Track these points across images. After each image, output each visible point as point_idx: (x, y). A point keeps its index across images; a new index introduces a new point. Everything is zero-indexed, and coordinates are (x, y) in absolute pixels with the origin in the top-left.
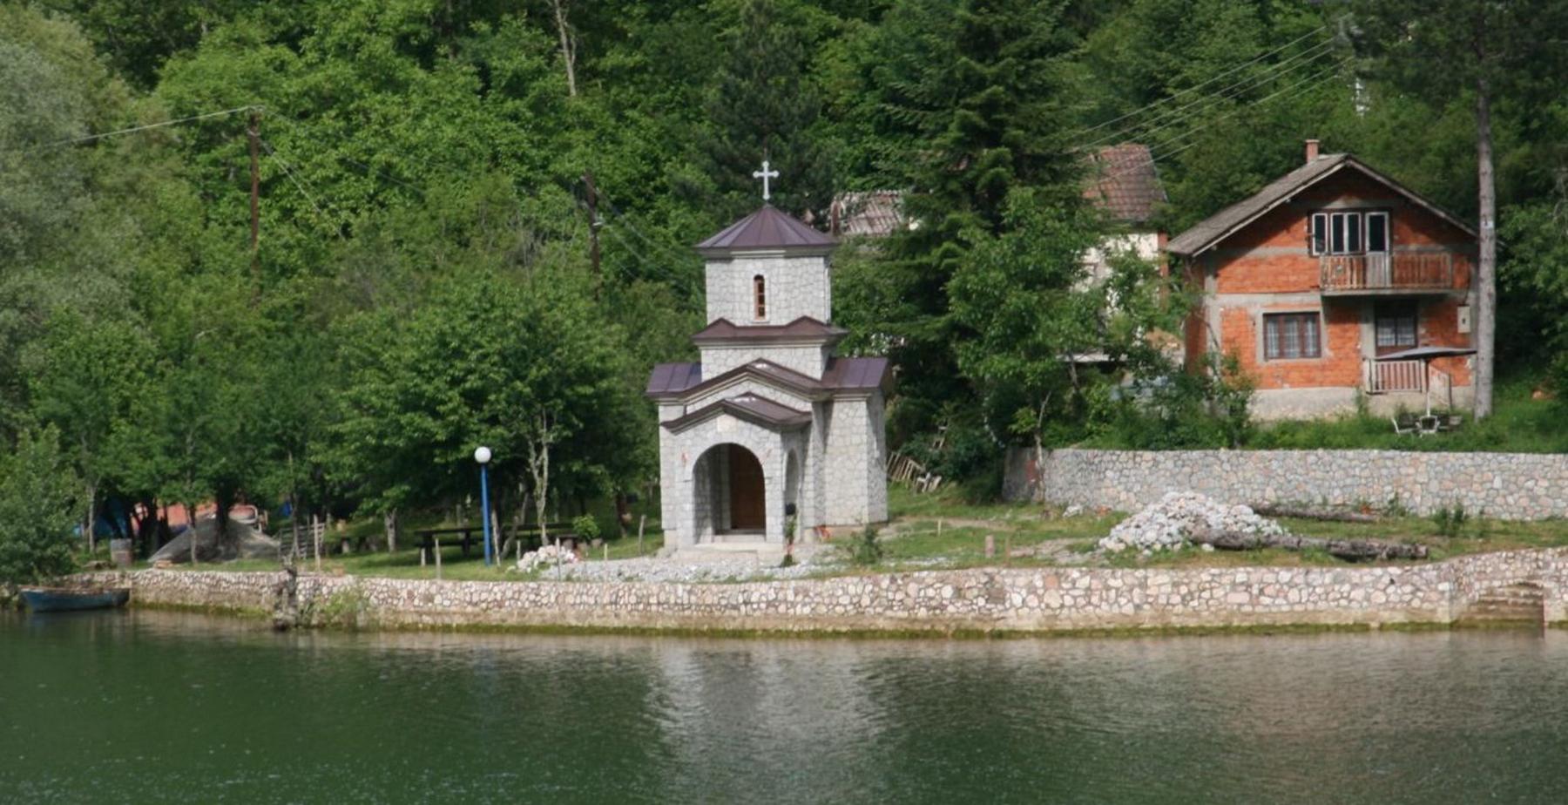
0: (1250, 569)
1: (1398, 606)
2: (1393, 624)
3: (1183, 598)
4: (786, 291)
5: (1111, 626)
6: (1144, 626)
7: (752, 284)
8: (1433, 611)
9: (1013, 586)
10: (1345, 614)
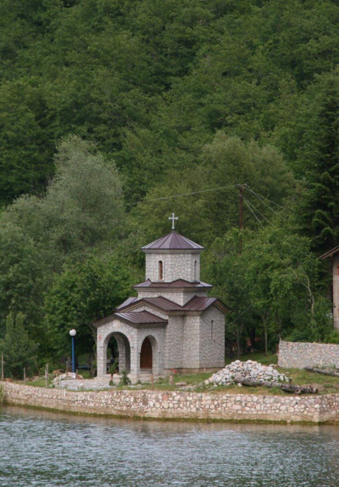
0: (242, 395)
1: (299, 414)
2: (296, 422)
3: (215, 406)
4: (171, 268)
5: (187, 417)
6: (200, 418)
7: (158, 264)
8: (312, 417)
9: (150, 398)
10: (277, 416)
